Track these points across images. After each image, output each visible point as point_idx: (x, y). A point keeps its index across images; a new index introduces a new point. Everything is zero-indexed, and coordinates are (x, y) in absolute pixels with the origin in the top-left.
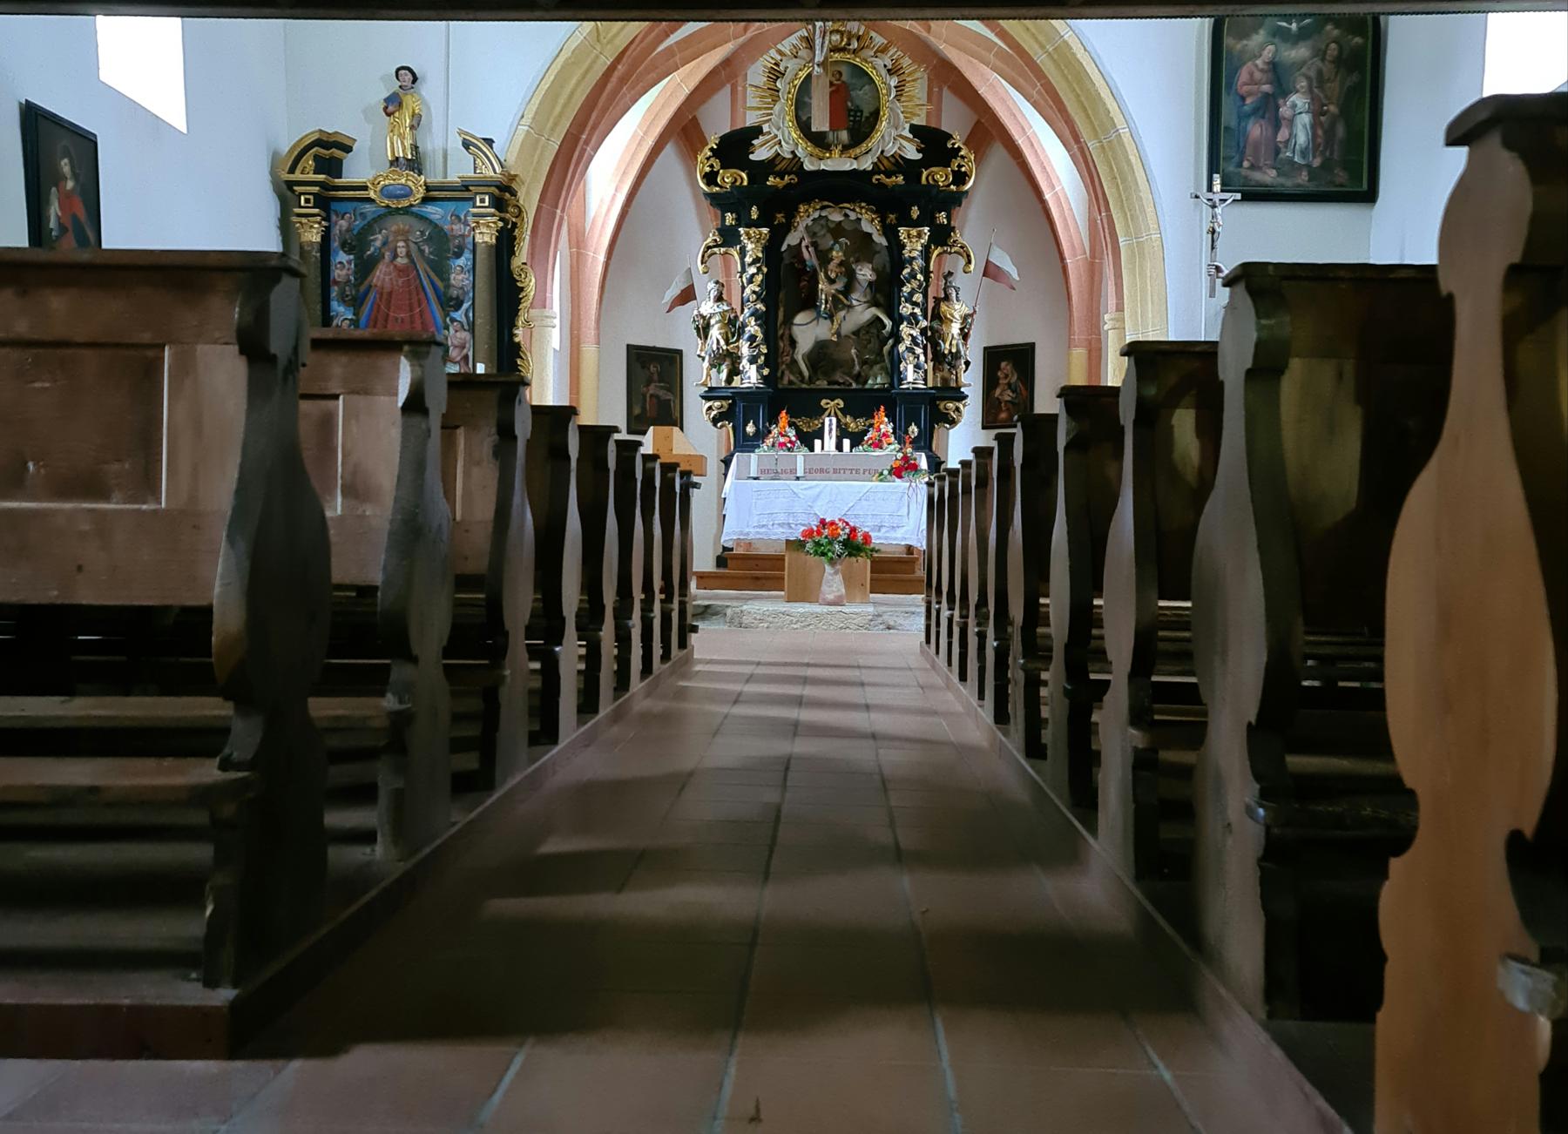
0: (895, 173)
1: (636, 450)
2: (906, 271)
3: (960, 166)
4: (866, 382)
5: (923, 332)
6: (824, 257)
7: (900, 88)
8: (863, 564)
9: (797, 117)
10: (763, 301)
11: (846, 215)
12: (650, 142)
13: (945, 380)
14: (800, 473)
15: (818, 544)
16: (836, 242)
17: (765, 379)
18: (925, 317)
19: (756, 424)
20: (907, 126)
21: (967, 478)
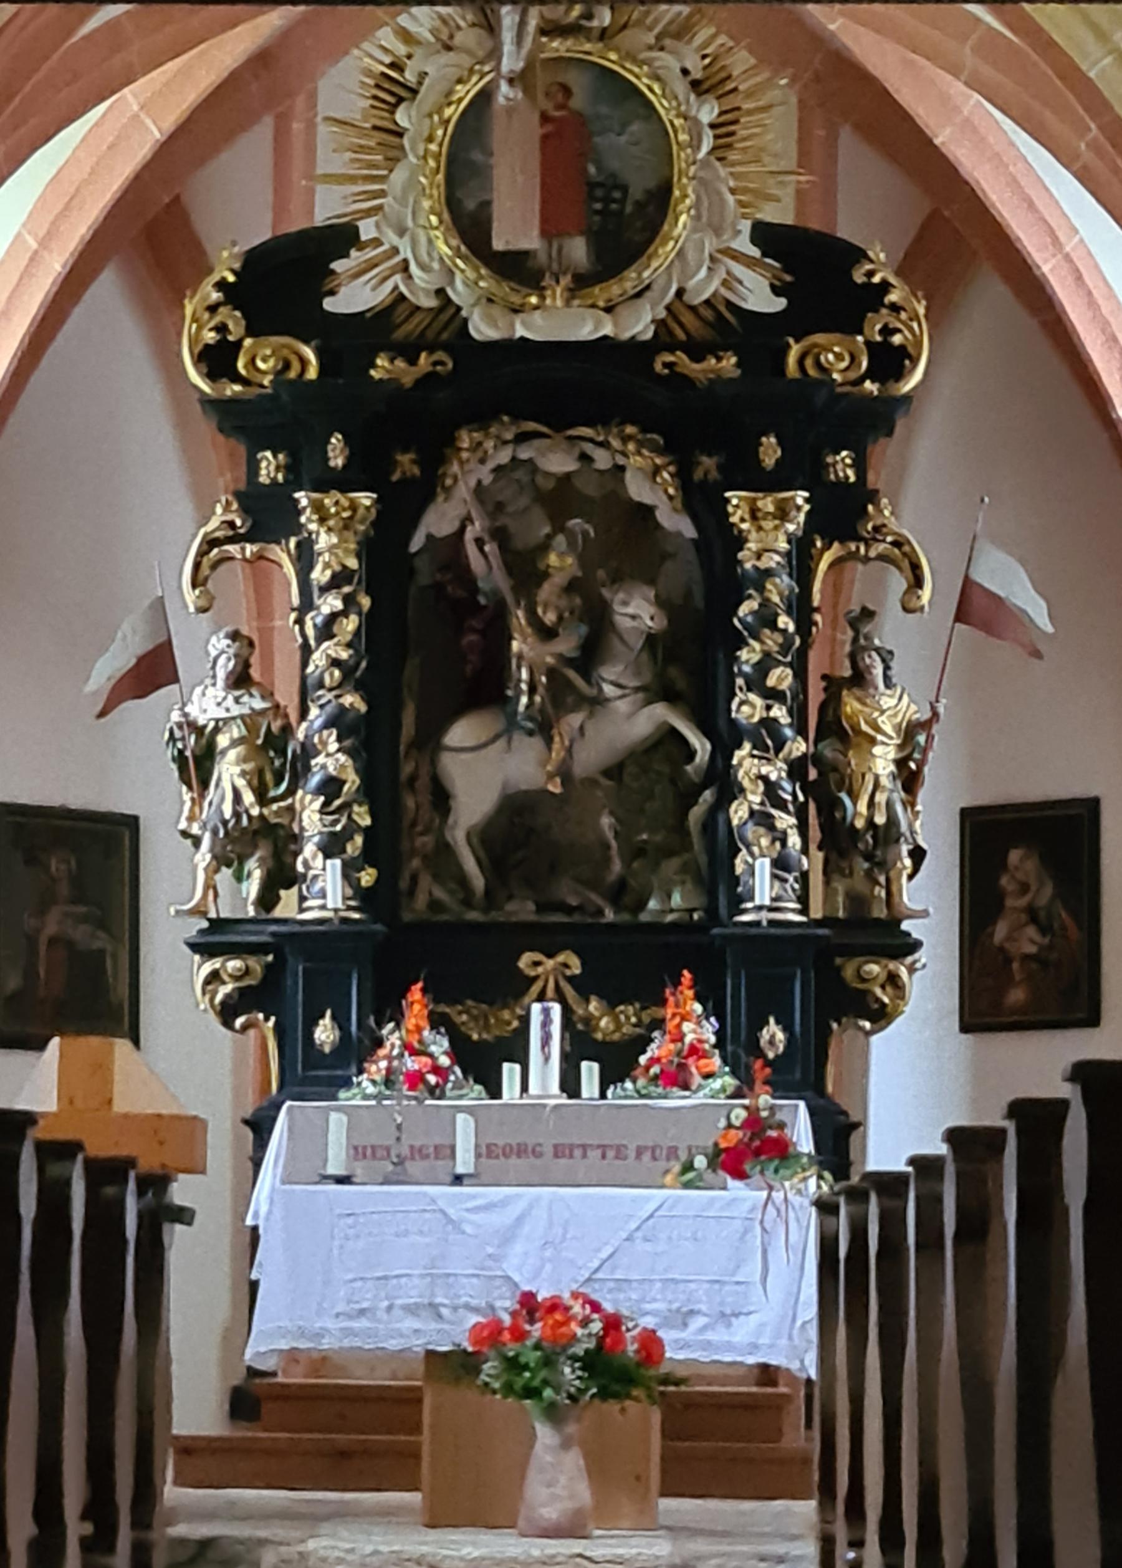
0: (712, 349)
1: (21, 1138)
2: (746, 609)
3: (887, 331)
4: (642, 905)
5: (796, 769)
6: (526, 571)
7: (723, 128)
8: (643, 1419)
9: (452, 202)
10: (360, 687)
11: (585, 458)
12: (56, 265)
13: (858, 902)
14: (464, 1163)
15: (514, 1365)
16: (559, 527)
17: (365, 898)
18: (801, 730)
19: (342, 1021)
20: (746, 226)
21: (930, 1207)
